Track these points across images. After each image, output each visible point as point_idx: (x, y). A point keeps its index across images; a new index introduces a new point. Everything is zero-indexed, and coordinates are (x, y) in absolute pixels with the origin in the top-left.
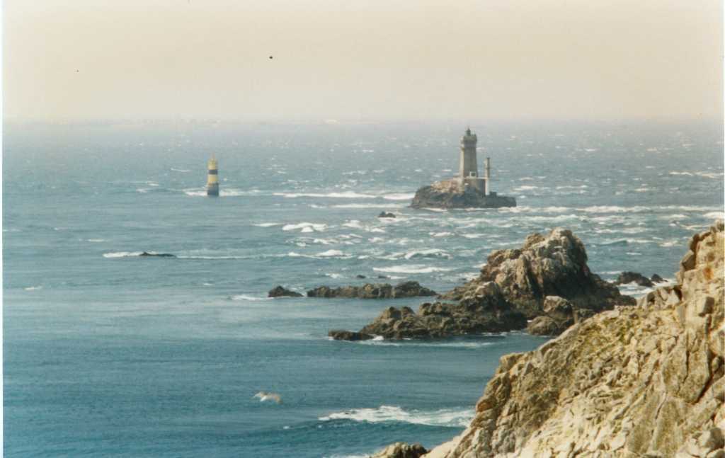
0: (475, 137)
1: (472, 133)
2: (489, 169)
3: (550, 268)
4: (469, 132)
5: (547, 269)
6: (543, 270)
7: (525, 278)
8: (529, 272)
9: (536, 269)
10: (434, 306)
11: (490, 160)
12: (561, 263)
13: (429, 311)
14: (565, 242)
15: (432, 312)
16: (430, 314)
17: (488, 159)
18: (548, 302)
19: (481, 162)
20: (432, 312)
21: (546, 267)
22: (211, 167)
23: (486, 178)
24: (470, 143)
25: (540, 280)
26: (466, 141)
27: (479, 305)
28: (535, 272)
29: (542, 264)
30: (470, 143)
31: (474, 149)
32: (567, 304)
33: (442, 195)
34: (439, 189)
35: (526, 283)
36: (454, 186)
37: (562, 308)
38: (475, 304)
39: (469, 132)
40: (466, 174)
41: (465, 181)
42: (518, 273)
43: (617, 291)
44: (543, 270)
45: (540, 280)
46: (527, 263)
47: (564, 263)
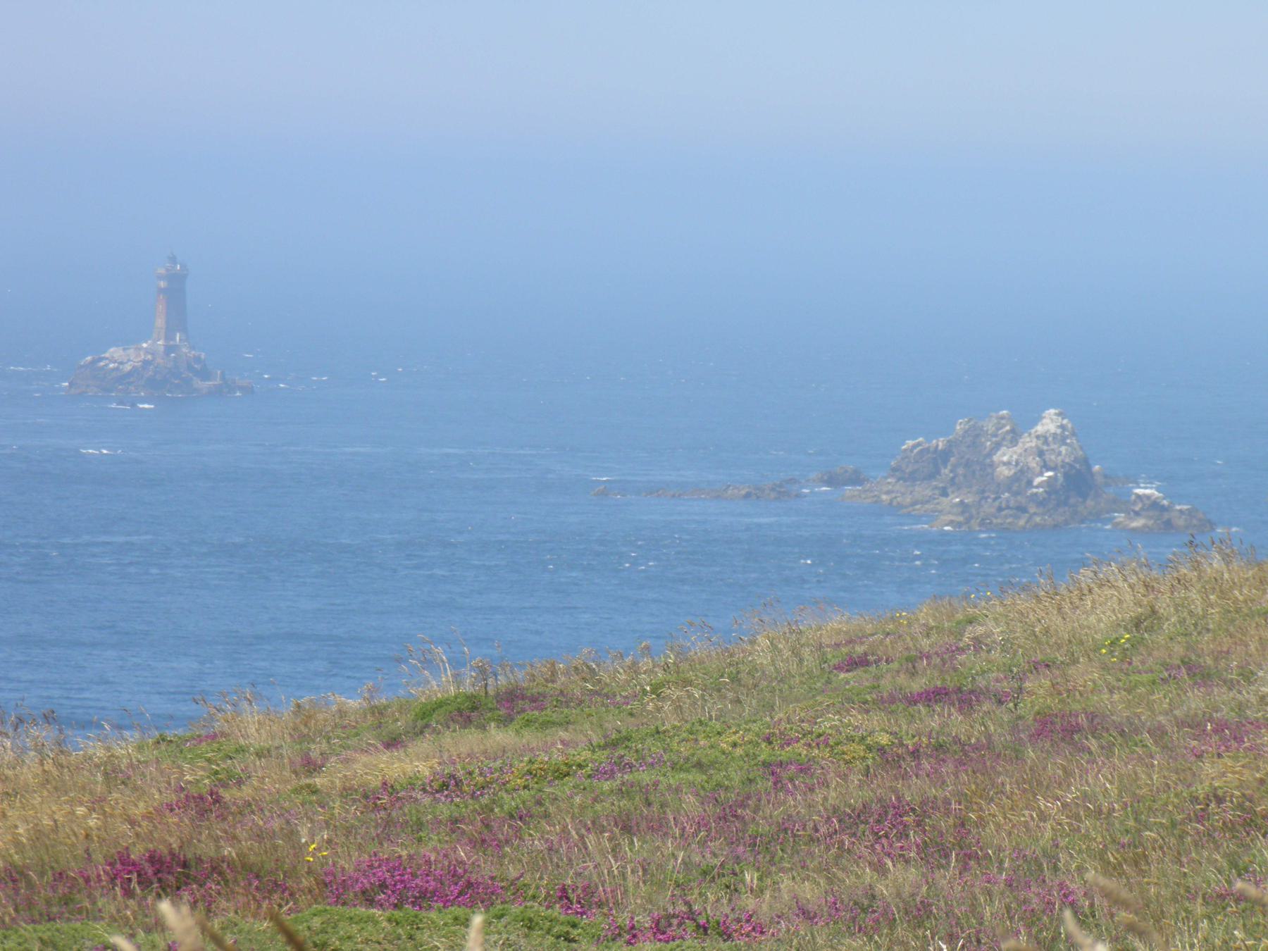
4: (173, 260)
13: (1004, 505)
18: (1138, 496)
20: (1008, 507)
29: (1060, 454)
34: (121, 363)
40: (169, 336)
41: (169, 349)
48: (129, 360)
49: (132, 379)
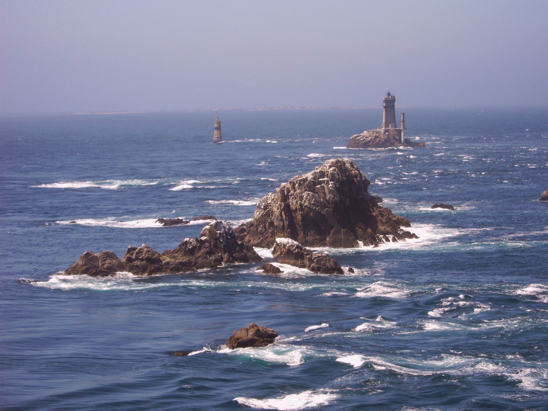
0: (393, 97)
1: (391, 94)
2: (404, 121)
3: (310, 203)
4: (389, 94)
5: (307, 204)
6: (301, 205)
7: (281, 215)
8: (287, 209)
9: (293, 203)
10: (141, 251)
11: (405, 115)
12: (324, 198)
14: (332, 174)
15: (137, 259)
16: (135, 260)
17: (403, 114)
19: (399, 118)
21: (305, 201)
22: (216, 125)
23: (402, 128)
24: (390, 103)
25: (299, 216)
26: (386, 101)
27: (200, 249)
28: (293, 207)
29: (301, 198)
30: (390, 103)
31: (393, 107)
32: (298, 247)
33: (369, 142)
34: (366, 137)
35: (282, 220)
36: (378, 135)
37: (292, 252)
38: (194, 248)
39: (389, 94)
40: (387, 125)
41: (386, 131)
42: (275, 209)
43: (239, 253)
44: (301, 205)
45: (299, 216)
46: (285, 197)
47: (328, 197)
48: (369, 136)
49: (370, 144)
